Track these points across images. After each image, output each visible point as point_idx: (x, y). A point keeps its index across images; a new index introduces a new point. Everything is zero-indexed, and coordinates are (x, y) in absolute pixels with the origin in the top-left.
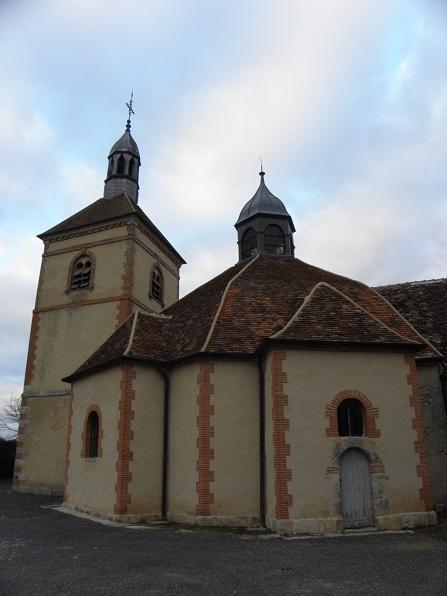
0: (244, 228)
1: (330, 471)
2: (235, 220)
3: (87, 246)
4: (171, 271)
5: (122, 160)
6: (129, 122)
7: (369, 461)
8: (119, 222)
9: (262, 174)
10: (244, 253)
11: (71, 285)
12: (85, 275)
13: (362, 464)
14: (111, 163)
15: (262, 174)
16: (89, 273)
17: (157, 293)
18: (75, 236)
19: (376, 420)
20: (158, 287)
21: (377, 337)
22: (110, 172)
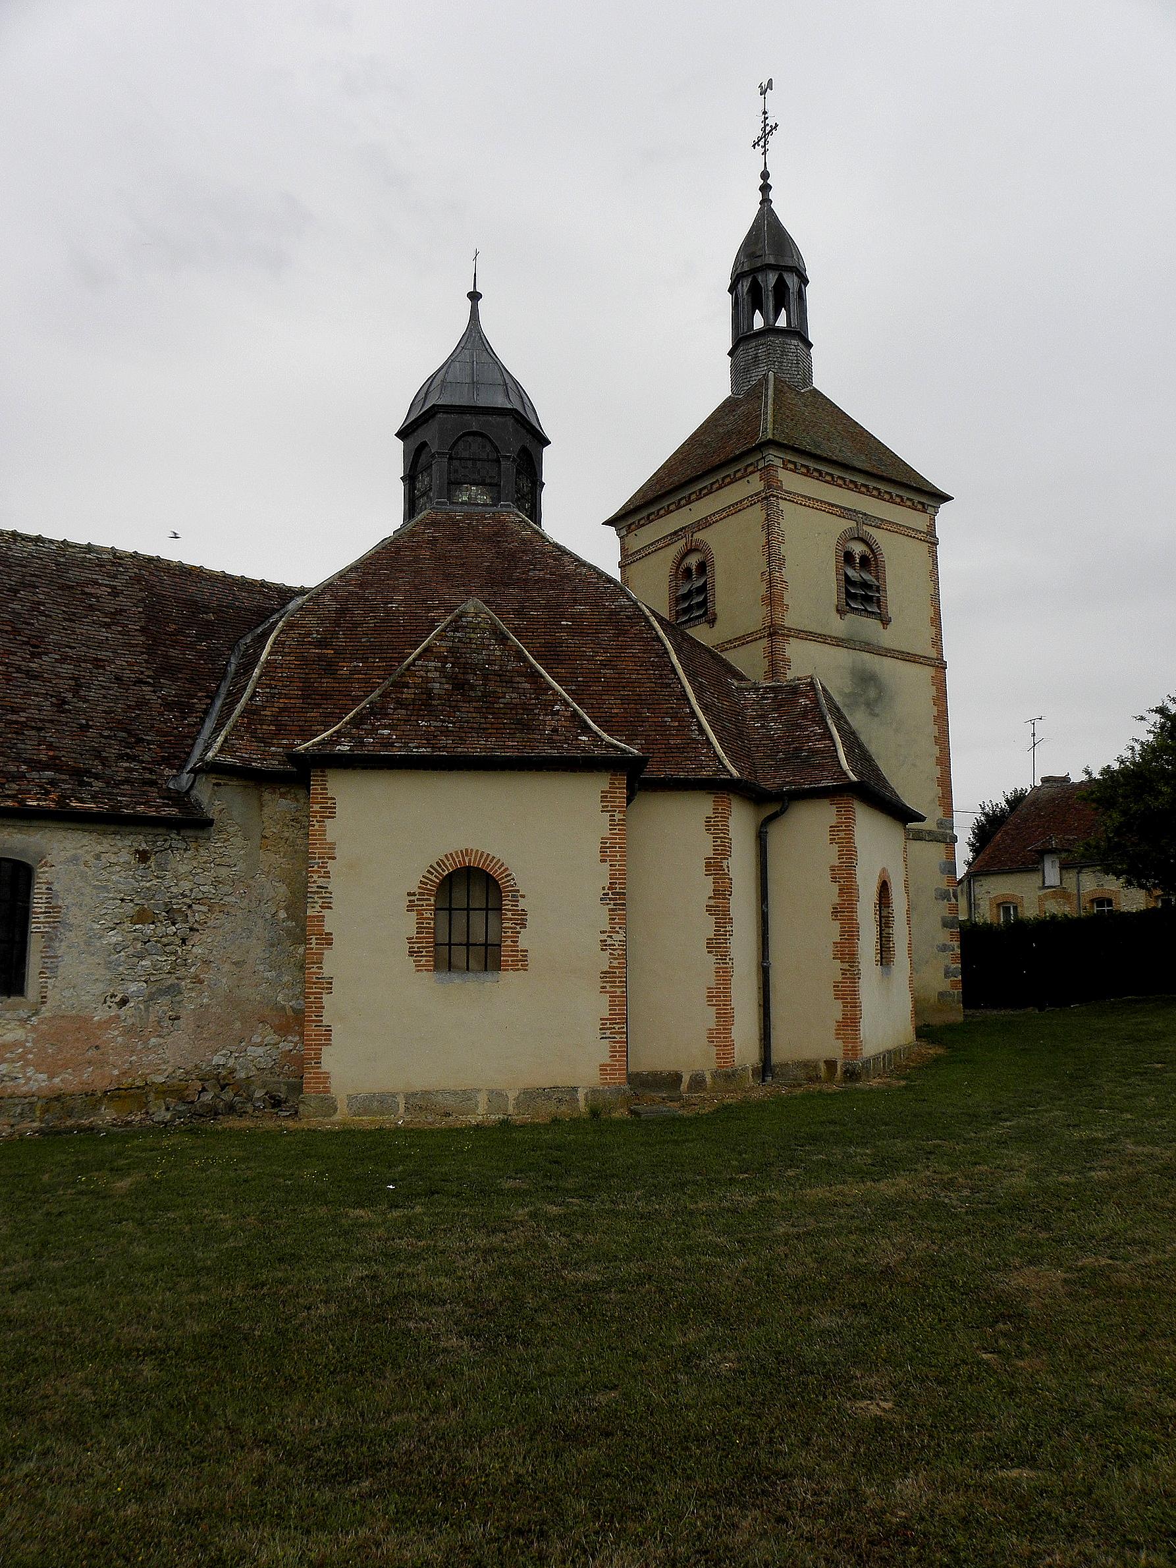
2: (398, 423)
6: (765, 175)
9: (474, 296)
10: (411, 508)
15: (474, 296)
16: (704, 587)
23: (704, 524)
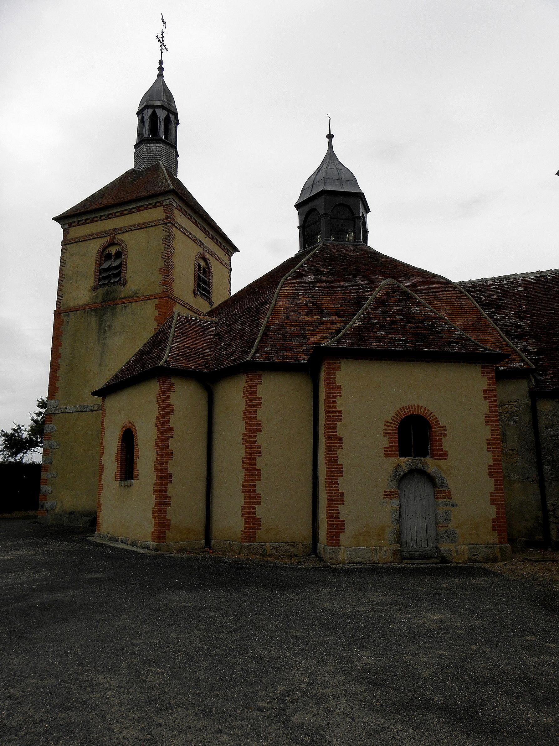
0: (306, 208)
1: (388, 495)
3: (115, 232)
4: (221, 261)
5: (154, 117)
6: (161, 62)
7: (434, 485)
8: (153, 201)
9: (330, 137)
11: (100, 280)
12: (116, 268)
13: (427, 489)
14: (141, 122)
15: (330, 137)
16: (120, 266)
17: (204, 289)
18: (101, 219)
19: (444, 439)
20: (204, 282)
21: (449, 344)
22: (140, 134)
23: (123, 231)
